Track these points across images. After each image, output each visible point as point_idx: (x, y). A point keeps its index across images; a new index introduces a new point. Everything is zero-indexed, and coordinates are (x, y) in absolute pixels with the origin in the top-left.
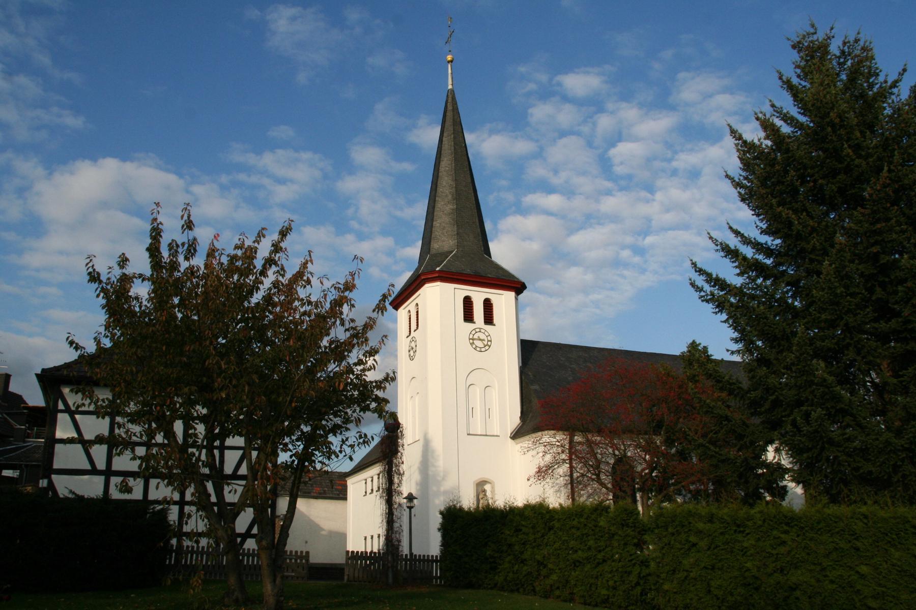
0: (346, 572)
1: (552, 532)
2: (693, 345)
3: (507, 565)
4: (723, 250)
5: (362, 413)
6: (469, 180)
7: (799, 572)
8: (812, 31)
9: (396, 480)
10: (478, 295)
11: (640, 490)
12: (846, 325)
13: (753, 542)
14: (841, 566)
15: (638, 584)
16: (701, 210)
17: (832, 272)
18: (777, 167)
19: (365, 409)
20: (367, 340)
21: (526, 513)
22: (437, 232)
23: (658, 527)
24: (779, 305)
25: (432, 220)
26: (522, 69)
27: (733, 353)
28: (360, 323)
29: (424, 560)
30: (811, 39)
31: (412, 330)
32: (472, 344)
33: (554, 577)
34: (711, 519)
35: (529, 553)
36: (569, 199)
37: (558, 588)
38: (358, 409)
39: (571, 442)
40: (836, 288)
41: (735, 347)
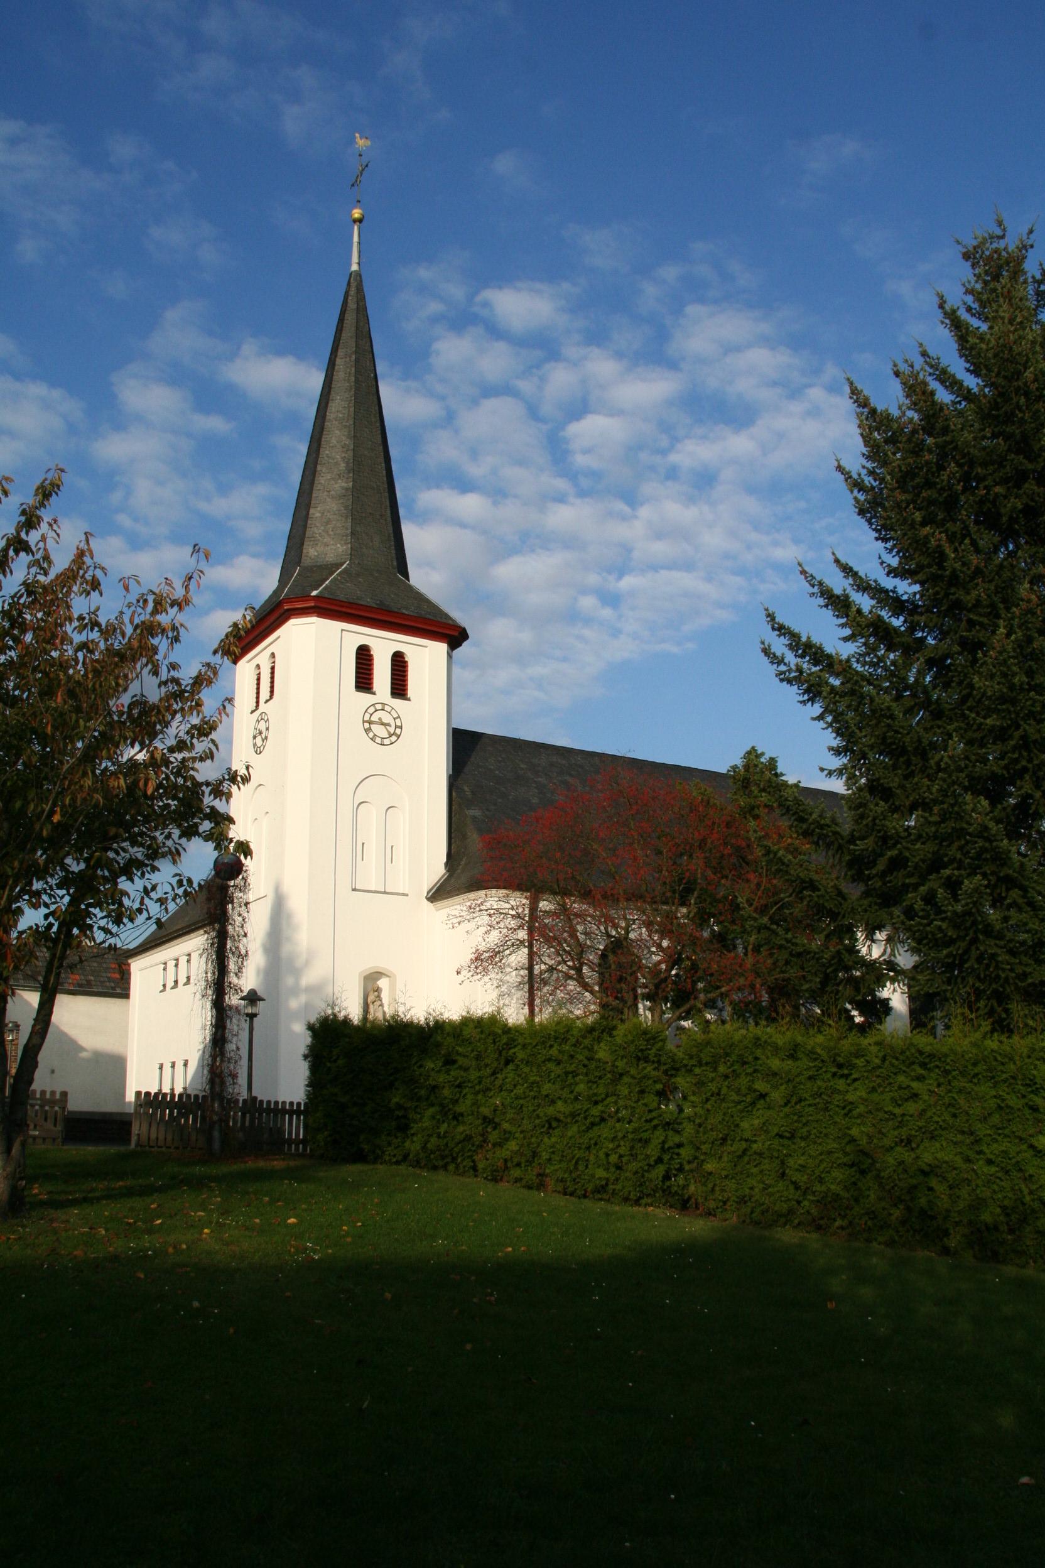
0: (135, 1130)
1: (511, 1067)
2: (752, 755)
3: (426, 1123)
4: (822, 594)
5: (184, 841)
6: (379, 439)
7: (938, 1145)
8: (999, 232)
9: (232, 966)
10: (384, 645)
11: (647, 997)
12: (1024, 737)
13: (864, 1094)
14: (1006, 1136)
15: (660, 1160)
16: (714, 540)
17: (1009, 648)
18: (927, 457)
19: (190, 832)
20: (199, 704)
21: (466, 1032)
22: (315, 528)
23: (700, 1064)
24: (914, 695)
25: (308, 506)
26: (424, 273)
27: (830, 773)
28: (187, 674)
29: (269, 1110)
30: (994, 246)
31: (262, 699)
32: (367, 731)
33: (513, 1145)
34: (793, 1052)
35: (468, 1102)
36: (495, 503)
37: (518, 1165)
38: (176, 833)
39: (533, 908)
40: (1014, 675)
41: (837, 762)
